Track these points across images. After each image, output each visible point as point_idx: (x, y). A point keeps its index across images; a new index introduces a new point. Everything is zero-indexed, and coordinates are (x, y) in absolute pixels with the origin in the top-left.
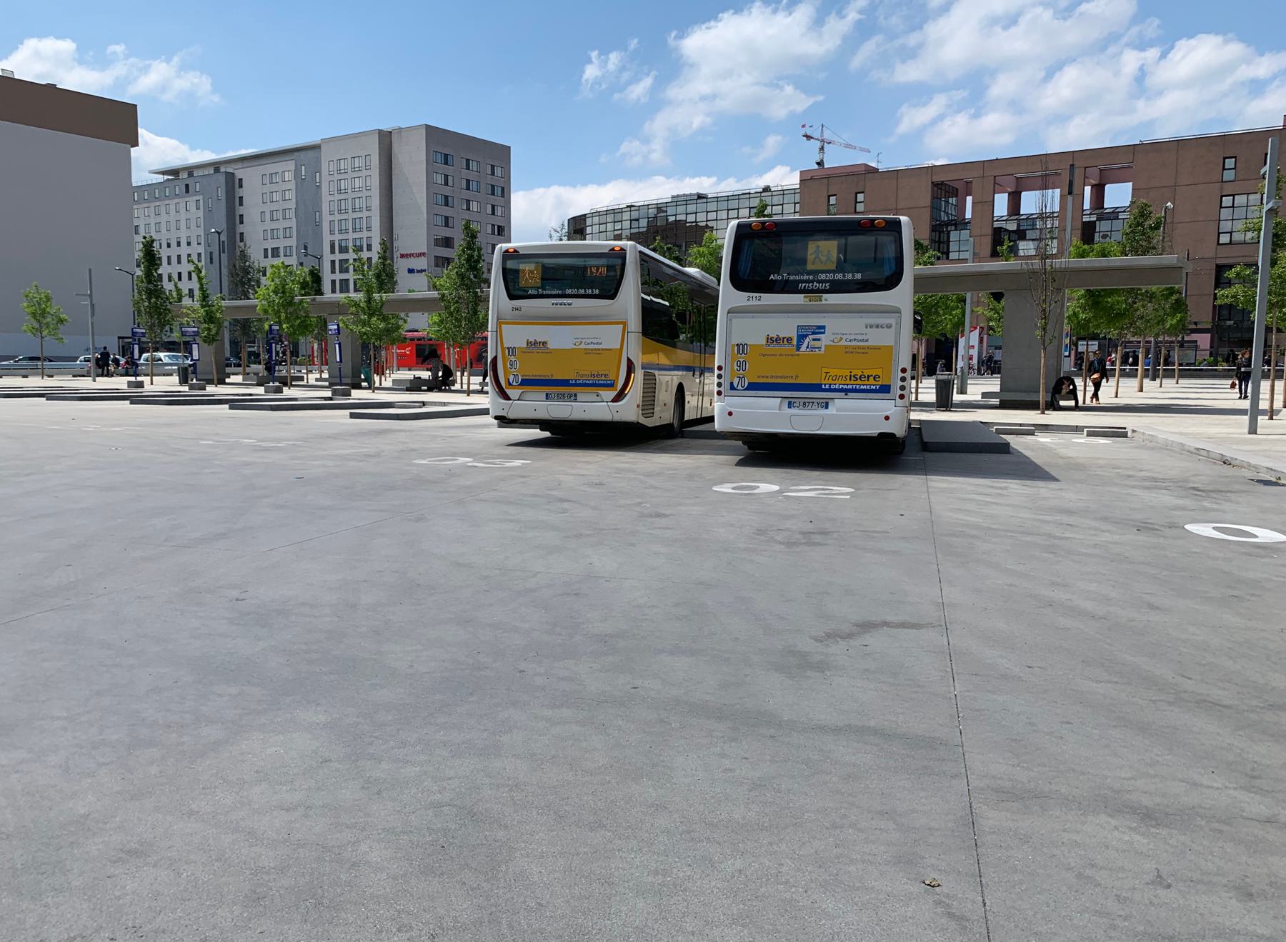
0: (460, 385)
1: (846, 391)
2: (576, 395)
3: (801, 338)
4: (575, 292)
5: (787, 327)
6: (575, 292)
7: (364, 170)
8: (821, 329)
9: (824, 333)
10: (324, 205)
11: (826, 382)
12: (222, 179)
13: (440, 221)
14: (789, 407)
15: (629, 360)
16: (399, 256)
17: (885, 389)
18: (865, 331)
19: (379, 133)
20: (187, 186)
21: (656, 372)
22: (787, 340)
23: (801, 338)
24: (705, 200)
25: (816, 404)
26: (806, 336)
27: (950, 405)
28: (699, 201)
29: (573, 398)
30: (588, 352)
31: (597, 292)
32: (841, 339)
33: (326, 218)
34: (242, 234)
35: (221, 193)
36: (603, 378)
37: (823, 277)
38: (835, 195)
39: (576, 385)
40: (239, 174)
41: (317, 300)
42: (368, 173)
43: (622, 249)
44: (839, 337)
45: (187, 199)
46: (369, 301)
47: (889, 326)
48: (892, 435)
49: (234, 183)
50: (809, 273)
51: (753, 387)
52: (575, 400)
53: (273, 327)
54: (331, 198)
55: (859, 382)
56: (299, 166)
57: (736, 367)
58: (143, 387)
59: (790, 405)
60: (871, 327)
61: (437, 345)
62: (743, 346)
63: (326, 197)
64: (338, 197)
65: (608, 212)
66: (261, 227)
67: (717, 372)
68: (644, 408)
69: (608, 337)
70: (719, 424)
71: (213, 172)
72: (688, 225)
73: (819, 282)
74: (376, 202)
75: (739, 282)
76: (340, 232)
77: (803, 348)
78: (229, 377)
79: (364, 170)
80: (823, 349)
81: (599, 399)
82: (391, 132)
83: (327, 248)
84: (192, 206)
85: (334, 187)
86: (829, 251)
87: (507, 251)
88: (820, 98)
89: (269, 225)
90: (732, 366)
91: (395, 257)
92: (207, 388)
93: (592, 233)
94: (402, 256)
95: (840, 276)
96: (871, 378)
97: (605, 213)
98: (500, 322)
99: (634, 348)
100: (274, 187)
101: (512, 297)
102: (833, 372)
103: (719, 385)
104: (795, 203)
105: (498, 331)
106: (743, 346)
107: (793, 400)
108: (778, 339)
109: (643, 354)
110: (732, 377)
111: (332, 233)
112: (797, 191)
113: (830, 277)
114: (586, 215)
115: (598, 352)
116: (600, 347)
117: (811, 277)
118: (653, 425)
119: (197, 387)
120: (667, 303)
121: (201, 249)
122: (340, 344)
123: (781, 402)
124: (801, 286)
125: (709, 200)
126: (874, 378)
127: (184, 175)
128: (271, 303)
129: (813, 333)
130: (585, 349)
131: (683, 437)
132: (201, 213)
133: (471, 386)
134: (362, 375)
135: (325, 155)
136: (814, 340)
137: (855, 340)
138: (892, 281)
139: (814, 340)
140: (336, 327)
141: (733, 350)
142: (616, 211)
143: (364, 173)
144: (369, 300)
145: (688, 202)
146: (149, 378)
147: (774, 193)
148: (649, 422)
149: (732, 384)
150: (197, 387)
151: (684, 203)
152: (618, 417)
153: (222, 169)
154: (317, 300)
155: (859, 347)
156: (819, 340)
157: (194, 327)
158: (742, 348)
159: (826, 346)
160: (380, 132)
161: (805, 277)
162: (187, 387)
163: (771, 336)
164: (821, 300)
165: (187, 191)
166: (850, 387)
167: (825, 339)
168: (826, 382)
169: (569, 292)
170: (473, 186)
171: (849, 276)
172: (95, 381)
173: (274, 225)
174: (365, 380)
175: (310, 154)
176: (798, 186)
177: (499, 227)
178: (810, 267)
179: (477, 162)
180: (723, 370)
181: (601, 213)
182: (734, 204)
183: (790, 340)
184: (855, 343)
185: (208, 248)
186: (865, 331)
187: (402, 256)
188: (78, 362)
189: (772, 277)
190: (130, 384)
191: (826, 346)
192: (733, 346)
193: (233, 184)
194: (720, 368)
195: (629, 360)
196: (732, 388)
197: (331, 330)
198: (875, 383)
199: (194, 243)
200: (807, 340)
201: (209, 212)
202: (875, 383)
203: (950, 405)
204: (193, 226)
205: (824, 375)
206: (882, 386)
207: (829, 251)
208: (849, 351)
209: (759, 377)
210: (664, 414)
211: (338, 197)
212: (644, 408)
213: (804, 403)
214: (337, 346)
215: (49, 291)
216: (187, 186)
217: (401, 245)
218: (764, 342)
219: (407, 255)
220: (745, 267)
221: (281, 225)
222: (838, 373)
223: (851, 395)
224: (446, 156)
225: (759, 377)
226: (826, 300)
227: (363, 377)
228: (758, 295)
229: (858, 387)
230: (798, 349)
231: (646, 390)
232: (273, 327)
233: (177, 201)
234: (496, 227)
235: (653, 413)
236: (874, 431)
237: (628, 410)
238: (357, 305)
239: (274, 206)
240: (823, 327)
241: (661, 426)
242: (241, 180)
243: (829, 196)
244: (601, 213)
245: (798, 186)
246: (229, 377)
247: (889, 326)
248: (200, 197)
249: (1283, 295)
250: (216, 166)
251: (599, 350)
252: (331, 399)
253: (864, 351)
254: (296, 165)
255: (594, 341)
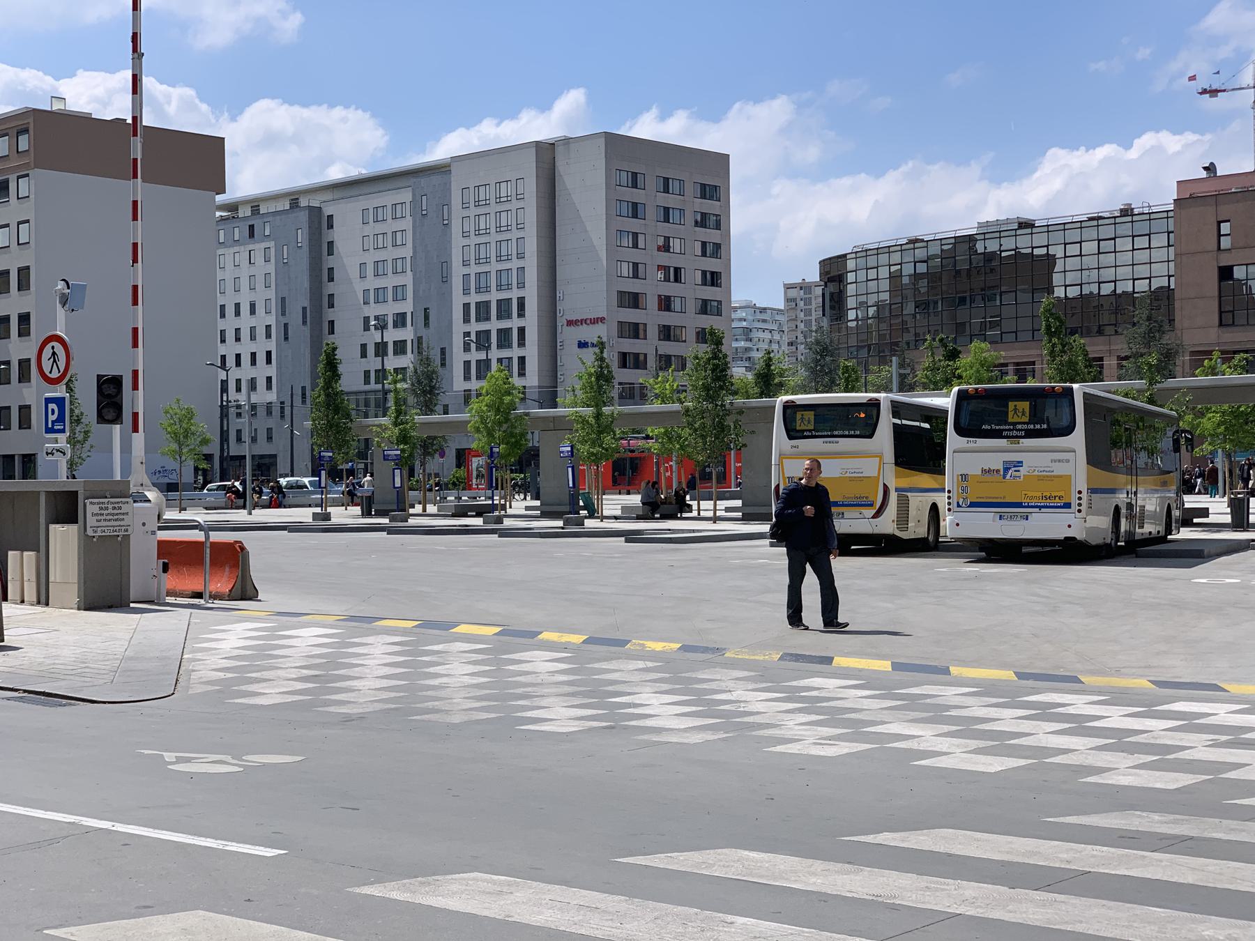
0: (697, 512)
1: (1040, 507)
2: (843, 513)
3: (1006, 470)
4: (841, 433)
5: (996, 462)
6: (841, 433)
7: (514, 201)
8: (1020, 463)
9: (1022, 466)
10: (454, 251)
11: (1025, 501)
12: (303, 217)
13: (626, 270)
14: (1000, 519)
15: (884, 484)
16: (565, 324)
17: (1068, 505)
18: (1050, 464)
19: (536, 146)
20: (252, 227)
21: (909, 494)
22: (996, 472)
23: (1006, 470)
24: (1029, 231)
25: (1019, 516)
26: (1010, 468)
27: (1245, 524)
28: (1019, 232)
29: (840, 516)
30: (852, 479)
31: (858, 433)
32: (1035, 470)
33: (457, 271)
34: (331, 296)
35: (302, 236)
36: (865, 499)
37: (1019, 427)
38: (1228, 221)
39: (843, 505)
40: (328, 211)
41: (532, 415)
42: (521, 204)
43: (877, 400)
44: (1032, 469)
45: (251, 247)
46: (597, 417)
47: (1068, 461)
48: (1074, 539)
49: (320, 223)
50: (1010, 424)
51: (973, 505)
52: (843, 518)
53: (494, 449)
54: (466, 242)
55: (1048, 501)
56: (418, 198)
57: (961, 491)
58: (330, 520)
59: (1001, 518)
60: (1055, 461)
61: (640, 458)
62: (965, 476)
63: (457, 241)
64: (475, 240)
65: (880, 251)
66: (359, 286)
67: (947, 494)
68: (898, 523)
69: (868, 468)
70: (950, 531)
71: (287, 207)
72: (1004, 254)
73: (1017, 430)
74: (532, 247)
75: (960, 431)
76: (478, 290)
77: (1008, 477)
78: (414, 507)
79: (514, 201)
80: (1022, 478)
81: (861, 516)
82: (553, 144)
83: (458, 314)
84: (259, 258)
85: (470, 226)
86: (1023, 409)
87: (787, 402)
88: (808, 566)
89: (372, 283)
90: (958, 491)
91: (559, 324)
92: (409, 520)
93: (856, 282)
94: (570, 323)
95: (1032, 427)
96: (1057, 498)
97: (875, 252)
98: (782, 456)
99: (892, 477)
100: (380, 228)
101: (791, 437)
102: (1030, 494)
103: (949, 504)
104: (1169, 233)
105: (780, 465)
106: (965, 476)
107: (1003, 514)
108: (989, 471)
109: (896, 478)
110: (958, 498)
111: (466, 291)
112: (1171, 214)
113: (1025, 427)
114: (845, 256)
115: (861, 479)
116: (861, 475)
117: (1012, 427)
118: (908, 538)
119: (398, 518)
120: (927, 426)
121: (271, 320)
122: (573, 468)
123: (994, 515)
124: (1005, 433)
125: (1035, 230)
126: (1059, 498)
127: (245, 212)
128: (483, 420)
129: (1015, 466)
130: (850, 477)
131: (938, 551)
132: (271, 268)
133: (717, 512)
134: (581, 501)
135: (457, 182)
136: (1015, 471)
137: (1044, 471)
138: (1068, 430)
139: (1015, 471)
140: (569, 449)
141: (958, 480)
142: (891, 249)
143: (515, 204)
144: (598, 416)
145: (1002, 234)
146: (696, 502)
147: (1135, 218)
148: (904, 535)
149: (958, 503)
150: (398, 518)
151: (997, 235)
152: (877, 531)
153: (303, 202)
154: (532, 415)
155: (1047, 476)
156: (1019, 471)
157: (397, 450)
158: (964, 477)
159: (1024, 475)
160: (538, 144)
161: (1007, 427)
162: (388, 520)
163: (985, 468)
164: (1019, 443)
165: (252, 235)
166: (1042, 504)
167: (1023, 471)
168: (1025, 501)
169: (836, 433)
170: (675, 216)
171: (1038, 427)
172: (251, 514)
173: (380, 283)
174: (584, 508)
175: (436, 179)
176: (1171, 207)
177: (713, 273)
178: (1010, 420)
179: (680, 180)
180: (1077, 491)
181: (869, 253)
182: (1073, 235)
183: (998, 471)
184: (1045, 473)
185: (281, 318)
186: (1050, 464)
187: (570, 323)
188: (205, 491)
189: (984, 427)
190: (315, 516)
191: (1024, 475)
192: (958, 475)
193: (320, 223)
194: (949, 492)
195: (884, 484)
196: (959, 506)
197: (563, 452)
198: (1060, 501)
199: (260, 309)
200: (1011, 471)
201: (283, 265)
202: (1060, 501)
203: (1245, 524)
204: (260, 285)
205: (1023, 496)
206: (1065, 504)
207: (1023, 409)
208: (1040, 478)
209: (977, 498)
210: (917, 529)
211: (475, 240)
212: (898, 523)
213: (1011, 516)
214: (570, 469)
215: (192, 407)
216: (252, 227)
217: (570, 307)
218: (980, 473)
219: (577, 321)
220: (964, 422)
221: (390, 282)
222: (1034, 494)
223: (1043, 510)
224: (635, 175)
225: (977, 498)
226: (1022, 443)
227: (581, 503)
228: (974, 439)
229: (1048, 504)
230: (1004, 478)
231: (899, 509)
232: (494, 449)
233: (236, 249)
234: (708, 274)
235: (907, 528)
236: (1061, 536)
237: (887, 524)
238: (584, 421)
239: (380, 255)
240: (1022, 462)
241: (910, 539)
242: (330, 217)
243: (1219, 223)
244: (869, 253)
245: (1171, 207)
246: (414, 507)
247: (1068, 461)
248: (272, 244)
249: (1253, 444)
250: (294, 198)
251: (860, 477)
252: (563, 528)
253: (1051, 478)
254: (414, 195)
255: (857, 471)
